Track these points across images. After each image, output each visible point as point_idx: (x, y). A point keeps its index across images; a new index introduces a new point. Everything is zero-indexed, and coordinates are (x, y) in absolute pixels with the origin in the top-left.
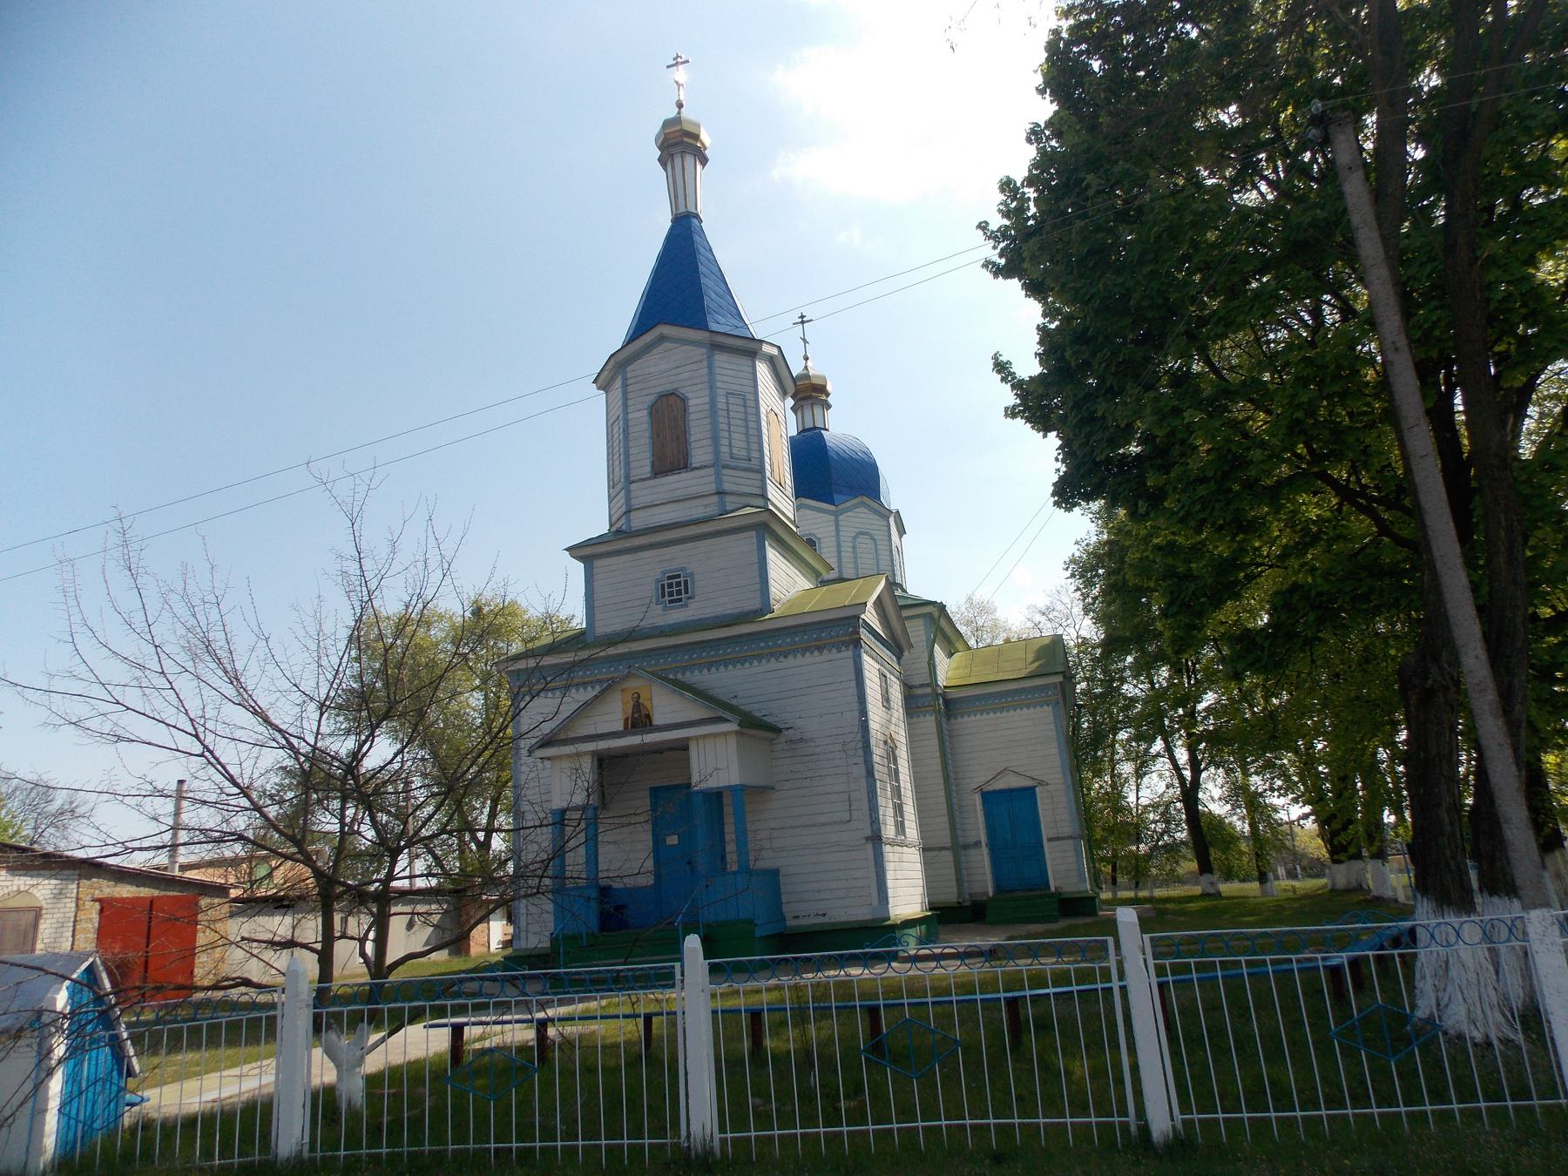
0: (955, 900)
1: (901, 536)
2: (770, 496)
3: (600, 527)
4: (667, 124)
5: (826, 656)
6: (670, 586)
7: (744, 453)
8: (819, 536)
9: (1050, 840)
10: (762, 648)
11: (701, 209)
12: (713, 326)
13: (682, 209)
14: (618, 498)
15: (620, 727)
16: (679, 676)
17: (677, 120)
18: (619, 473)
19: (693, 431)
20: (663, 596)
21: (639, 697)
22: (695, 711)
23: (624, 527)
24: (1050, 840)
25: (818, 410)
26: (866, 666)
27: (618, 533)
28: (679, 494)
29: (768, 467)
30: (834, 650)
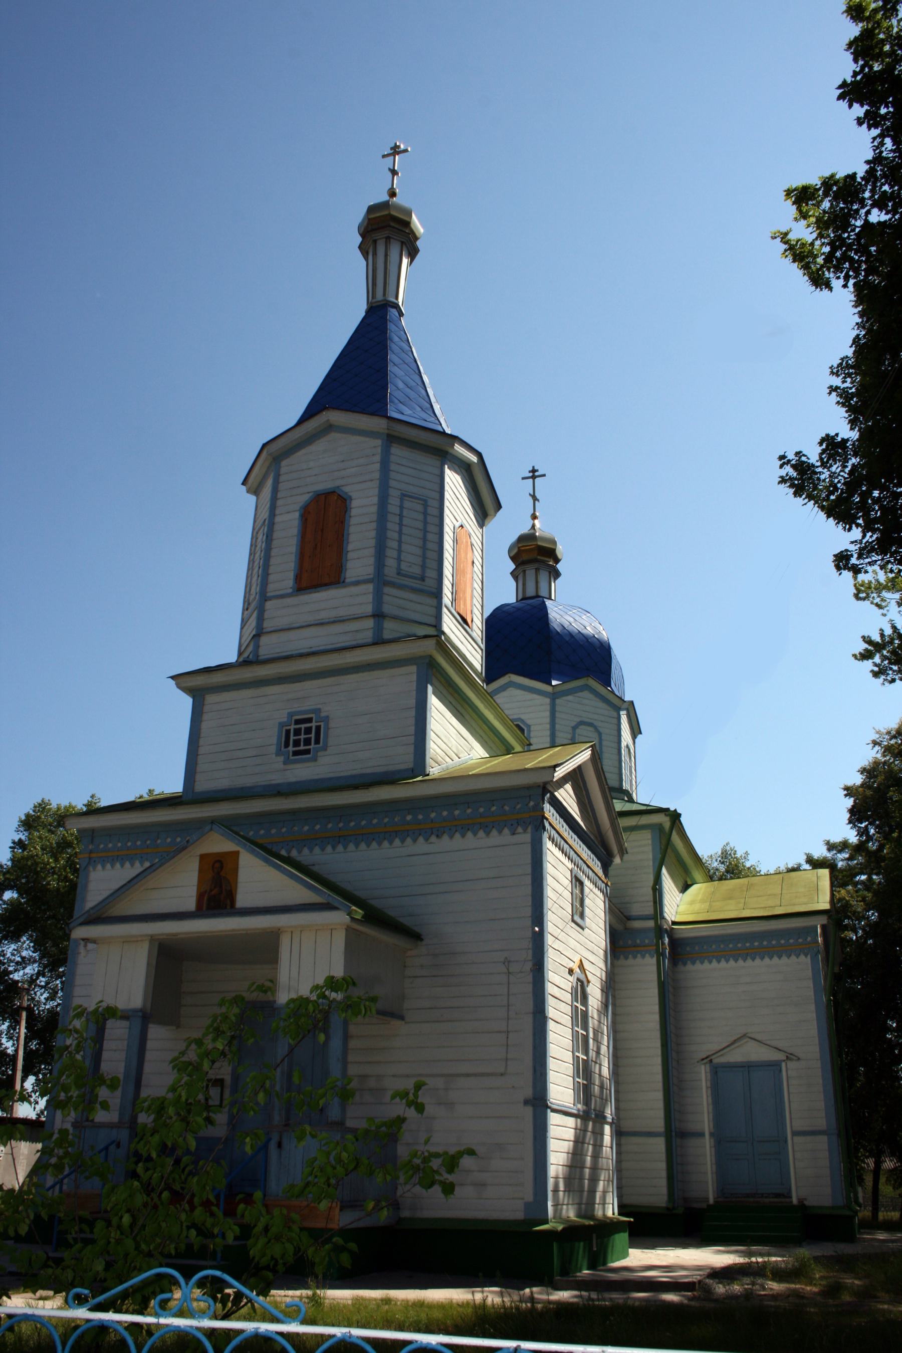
0: (664, 1205)
2: (445, 628)
3: (232, 658)
5: (495, 838)
6: (297, 732)
7: (417, 570)
8: (529, 722)
9: (795, 1133)
13: (379, 296)
15: (190, 904)
16: (294, 853)
17: (385, 205)
18: (255, 589)
19: (352, 538)
20: (287, 745)
21: (222, 867)
24: (795, 1133)
25: (543, 576)
28: (324, 616)
30: (506, 831)
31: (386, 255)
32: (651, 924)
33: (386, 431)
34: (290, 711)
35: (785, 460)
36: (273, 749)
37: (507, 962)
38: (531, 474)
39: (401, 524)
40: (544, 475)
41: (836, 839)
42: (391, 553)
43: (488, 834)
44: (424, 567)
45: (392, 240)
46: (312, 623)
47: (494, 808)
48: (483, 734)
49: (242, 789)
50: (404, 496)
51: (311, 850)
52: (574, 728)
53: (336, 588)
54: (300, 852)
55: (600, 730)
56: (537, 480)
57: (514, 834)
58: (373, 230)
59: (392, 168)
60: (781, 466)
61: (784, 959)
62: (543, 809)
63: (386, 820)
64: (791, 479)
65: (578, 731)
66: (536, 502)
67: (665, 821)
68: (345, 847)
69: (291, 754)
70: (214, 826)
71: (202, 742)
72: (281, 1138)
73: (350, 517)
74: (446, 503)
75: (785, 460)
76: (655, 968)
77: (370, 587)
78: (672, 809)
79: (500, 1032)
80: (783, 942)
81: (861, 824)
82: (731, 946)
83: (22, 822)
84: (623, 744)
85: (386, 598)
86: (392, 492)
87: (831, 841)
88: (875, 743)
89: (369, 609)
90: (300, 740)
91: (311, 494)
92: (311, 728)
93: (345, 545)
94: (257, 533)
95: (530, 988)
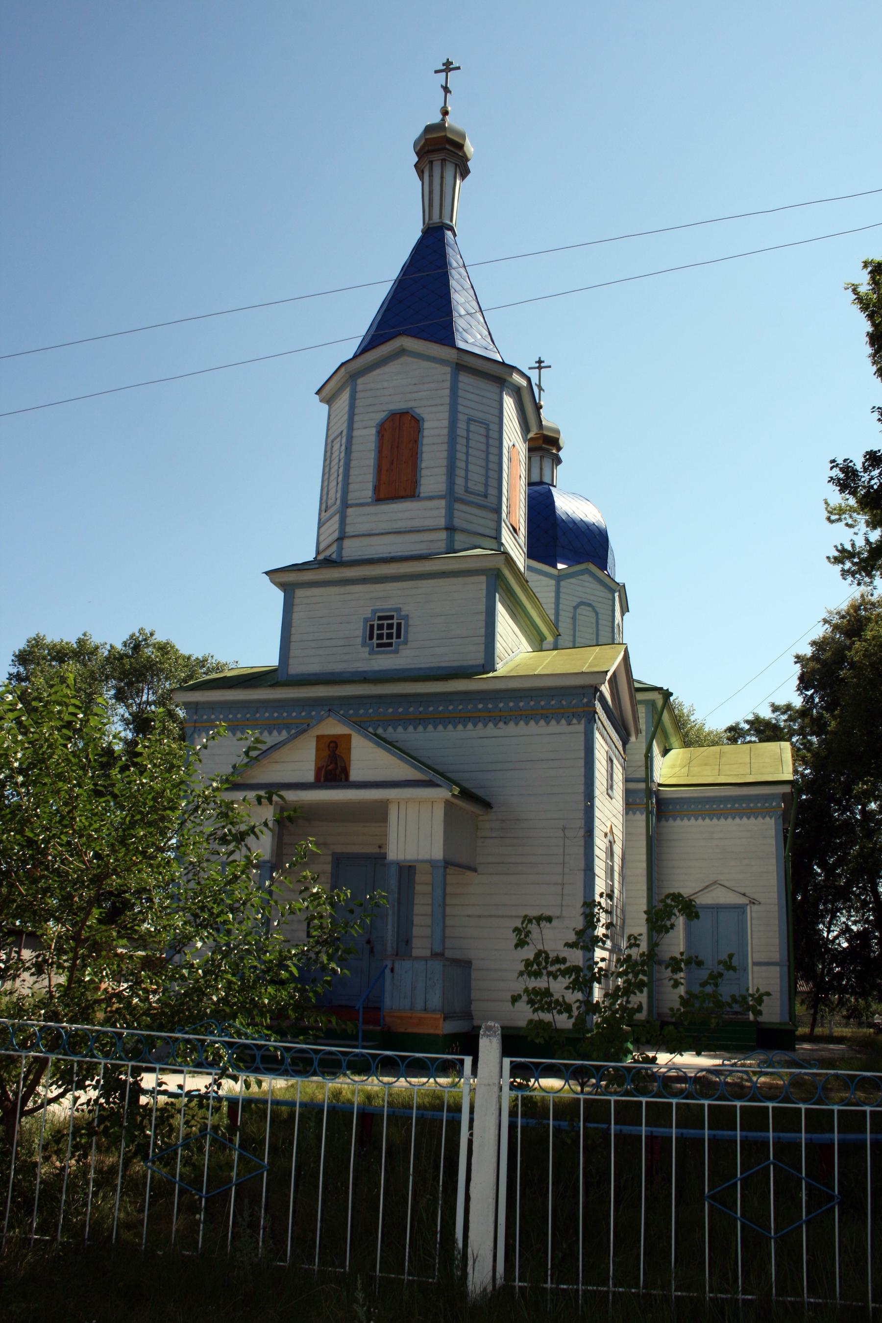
1: (623, 614)
2: (503, 541)
3: (309, 555)
4: (429, 129)
5: (554, 727)
6: (380, 627)
7: (480, 488)
9: (755, 964)
10: (480, 711)
11: (457, 221)
12: (461, 344)
13: (436, 218)
14: (332, 521)
15: (310, 776)
18: (335, 494)
19: (425, 456)
20: (371, 638)
21: (336, 747)
22: (402, 770)
23: (334, 556)
24: (755, 964)
26: (597, 745)
27: (323, 562)
28: (401, 525)
29: (504, 508)
31: (442, 178)
32: (642, 786)
33: (456, 361)
34: (372, 608)
35: (835, 464)
36: (359, 640)
37: (564, 829)
38: (537, 365)
39: (467, 446)
40: (550, 367)
41: (781, 702)
42: (460, 473)
43: (548, 723)
44: (486, 485)
45: (447, 162)
46: (390, 531)
47: (553, 702)
48: (527, 629)
49: (332, 674)
50: (470, 420)
51: (395, 729)
52: (575, 608)
53: (412, 501)
54: (385, 730)
55: (598, 609)
56: (542, 370)
57: (570, 724)
58: (429, 152)
59: (444, 85)
60: (832, 468)
61: (752, 820)
62: (595, 705)
63: (461, 707)
64: (839, 479)
65: (579, 611)
66: (542, 392)
67: (659, 699)
68: (425, 728)
69: (375, 646)
70: (331, 713)
71: (293, 631)
72: (393, 964)
73: (423, 437)
74: (505, 428)
75: (835, 464)
76: (644, 824)
77: (443, 503)
78: (665, 688)
79: (557, 884)
80: (752, 805)
81: (808, 691)
82: (707, 806)
83: (16, 656)
84: (616, 622)
85: (456, 513)
86: (461, 417)
87: (776, 704)
88: (825, 621)
89: (442, 522)
90: (383, 634)
91: (387, 412)
92: (393, 624)
93: (419, 462)
94: (332, 442)
95: (581, 850)
